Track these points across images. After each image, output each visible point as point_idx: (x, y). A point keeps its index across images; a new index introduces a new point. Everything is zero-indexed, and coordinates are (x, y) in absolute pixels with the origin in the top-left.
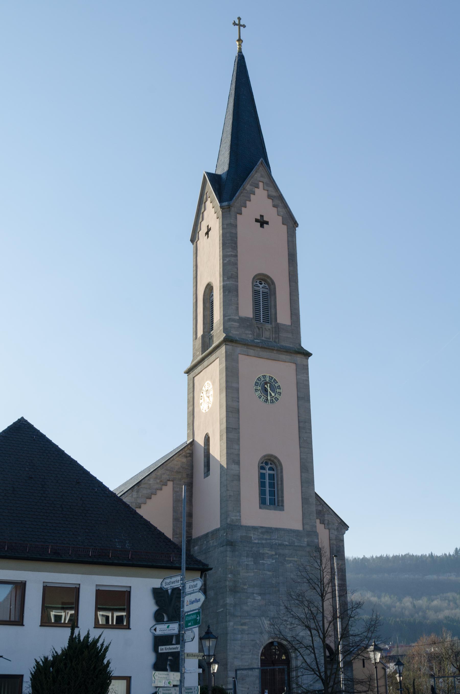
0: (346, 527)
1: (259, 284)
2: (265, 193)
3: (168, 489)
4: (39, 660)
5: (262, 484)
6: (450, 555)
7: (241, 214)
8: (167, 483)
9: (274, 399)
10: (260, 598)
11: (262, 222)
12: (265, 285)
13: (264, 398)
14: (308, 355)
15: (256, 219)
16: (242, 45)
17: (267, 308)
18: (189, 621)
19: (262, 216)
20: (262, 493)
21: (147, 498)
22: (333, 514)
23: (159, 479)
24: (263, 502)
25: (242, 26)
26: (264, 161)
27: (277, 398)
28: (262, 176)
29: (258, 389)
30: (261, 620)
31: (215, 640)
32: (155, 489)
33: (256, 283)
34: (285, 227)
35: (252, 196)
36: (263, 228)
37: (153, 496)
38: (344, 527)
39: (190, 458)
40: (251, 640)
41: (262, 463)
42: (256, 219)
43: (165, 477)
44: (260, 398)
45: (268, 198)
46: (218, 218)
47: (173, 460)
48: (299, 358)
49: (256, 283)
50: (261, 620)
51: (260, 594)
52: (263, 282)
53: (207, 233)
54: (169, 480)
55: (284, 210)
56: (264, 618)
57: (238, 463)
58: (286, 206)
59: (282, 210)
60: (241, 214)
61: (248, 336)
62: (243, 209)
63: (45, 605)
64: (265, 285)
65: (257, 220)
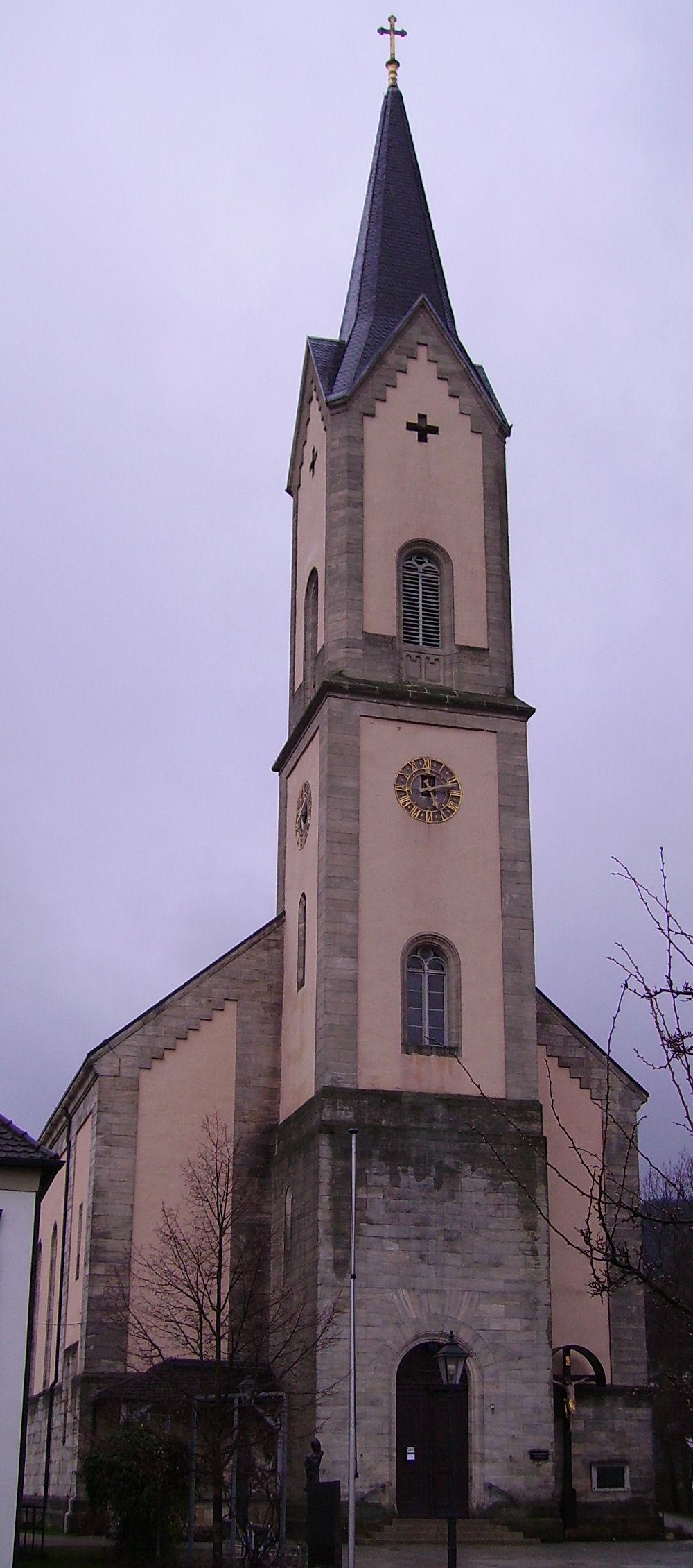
1: (416, 564)
3: (227, 1020)
7: (373, 416)
9: (442, 812)
10: (396, 1247)
11: (422, 429)
12: (429, 565)
13: (418, 810)
14: (527, 712)
15: (408, 423)
16: (398, 71)
17: (433, 614)
19: (422, 417)
21: (178, 1038)
23: (205, 997)
25: (397, 33)
26: (427, 299)
27: (450, 809)
28: (424, 333)
29: (406, 790)
30: (398, 1296)
32: (196, 1019)
33: (409, 562)
34: (478, 439)
36: (426, 441)
40: (373, 1339)
42: (408, 423)
43: (219, 993)
44: (409, 810)
47: (237, 956)
48: (504, 724)
49: (409, 562)
50: (398, 1296)
51: (397, 1239)
55: (475, 400)
56: (405, 1292)
57: (353, 953)
59: (469, 400)
61: (383, 675)
62: (379, 406)
63: (457, 1383)
64: (429, 565)
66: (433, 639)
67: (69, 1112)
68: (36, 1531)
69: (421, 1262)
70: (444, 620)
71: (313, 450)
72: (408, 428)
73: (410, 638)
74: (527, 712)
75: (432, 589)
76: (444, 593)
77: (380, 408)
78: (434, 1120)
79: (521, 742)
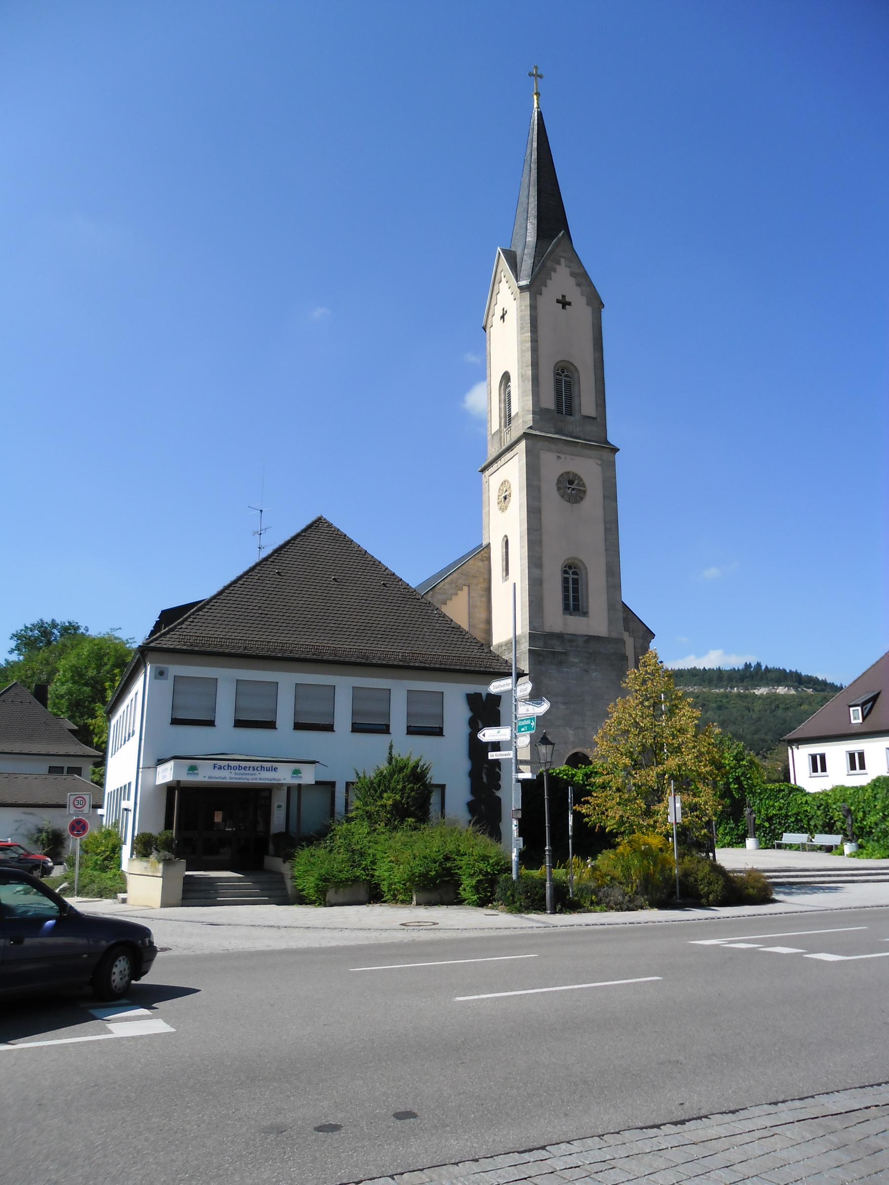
0: (650, 635)
2: (568, 270)
4: (421, 763)
5: (566, 589)
6: (739, 669)
8: (462, 588)
11: (564, 303)
14: (615, 450)
17: (570, 398)
18: (523, 726)
20: (566, 598)
22: (638, 621)
24: (566, 608)
31: (552, 746)
35: (553, 274)
37: (453, 597)
38: (650, 635)
39: (486, 562)
41: (565, 567)
45: (571, 276)
46: (515, 299)
48: (605, 454)
51: (564, 703)
52: (566, 371)
53: (503, 317)
54: (465, 585)
58: (591, 284)
60: (541, 294)
62: (544, 289)
65: (558, 301)
66: (570, 413)
67: (76, 728)
68: (794, 747)
69: (101, 832)
70: (575, 402)
71: (503, 309)
72: (571, 303)
73: (559, 411)
74: (615, 450)
75: (569, 385)
76: (575, 390)
77: (544, 289)
78: (577, 646)
79: (613, 464)
